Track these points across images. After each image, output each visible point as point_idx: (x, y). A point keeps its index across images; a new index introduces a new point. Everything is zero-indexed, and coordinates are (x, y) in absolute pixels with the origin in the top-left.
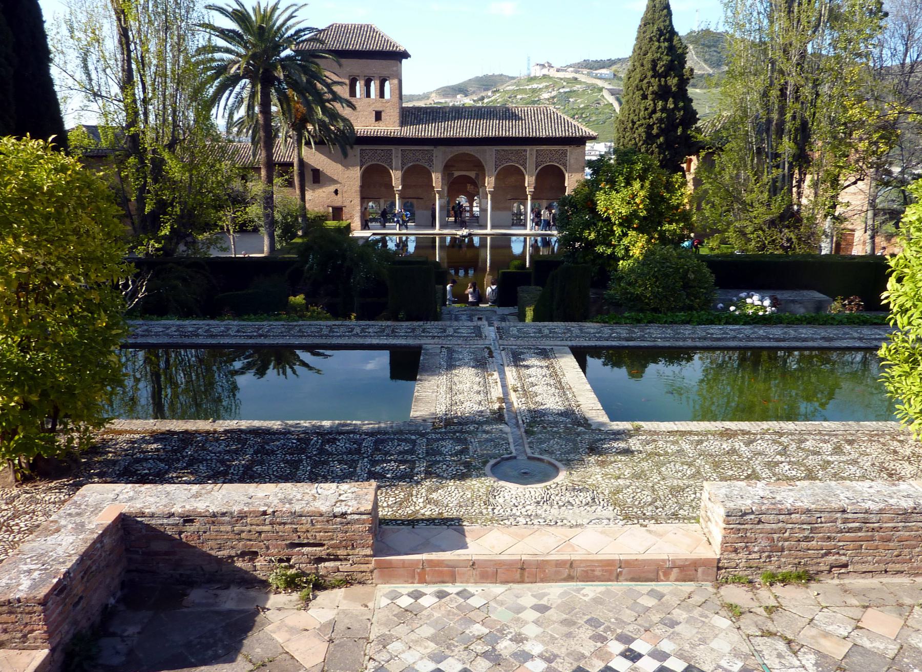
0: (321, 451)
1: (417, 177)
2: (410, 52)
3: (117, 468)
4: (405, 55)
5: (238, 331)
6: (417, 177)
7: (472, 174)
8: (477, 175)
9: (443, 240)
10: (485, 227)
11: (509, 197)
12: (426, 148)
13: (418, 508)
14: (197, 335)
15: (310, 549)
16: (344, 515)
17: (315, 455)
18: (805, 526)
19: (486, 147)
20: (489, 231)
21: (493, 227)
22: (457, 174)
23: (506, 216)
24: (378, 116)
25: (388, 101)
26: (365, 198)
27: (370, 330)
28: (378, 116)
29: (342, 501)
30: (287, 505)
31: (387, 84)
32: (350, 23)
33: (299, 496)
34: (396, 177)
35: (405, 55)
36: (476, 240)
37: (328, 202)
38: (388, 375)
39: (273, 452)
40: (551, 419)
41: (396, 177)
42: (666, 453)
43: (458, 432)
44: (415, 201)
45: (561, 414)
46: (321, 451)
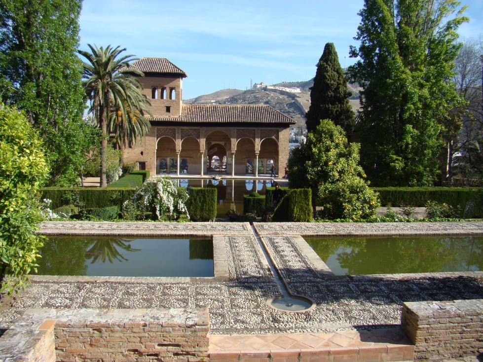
0: (164, 294)
1: (191, 145)
2: (186, 74)
3: (40, 302)
4: (182, 75)
5: (99, 227)
6: (191, 145)
7: (222, 143)
8: (225, 144)
9: (205, 181)
10: (231, 174)
11: (244, 157)
12: (196, 128)
13: (231, 325)
14: (75, 229)
15: (172, 347)
16: (191, 326)
17: (161, 296)
18: (463, 325)
19: (230, 128)
20: (234, 176)
21: (235, 174)
22: (213, 143)
23: (242, 167)
24: (168, 109)
25: (174, 101)
26: (159, 156)
27: (179, 226)
28: (168, 109)
29: (189, 318)
30: (156, 320)
31: (173, 91)
32: (160, 57)
33: (163, 316)
34: (179, 144)
35: (182, 75)
36: (224, 183)
37: (137, 159)
38: (189, 257)
39: (135, 294)
40: (300, 274)
41: (179, 144)
42: (372, 291)
43: (246, 282)
44: (188, 159)
45: (305, 271)
46: (164, 294)
